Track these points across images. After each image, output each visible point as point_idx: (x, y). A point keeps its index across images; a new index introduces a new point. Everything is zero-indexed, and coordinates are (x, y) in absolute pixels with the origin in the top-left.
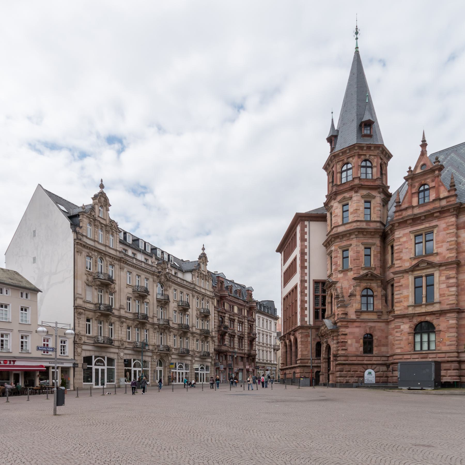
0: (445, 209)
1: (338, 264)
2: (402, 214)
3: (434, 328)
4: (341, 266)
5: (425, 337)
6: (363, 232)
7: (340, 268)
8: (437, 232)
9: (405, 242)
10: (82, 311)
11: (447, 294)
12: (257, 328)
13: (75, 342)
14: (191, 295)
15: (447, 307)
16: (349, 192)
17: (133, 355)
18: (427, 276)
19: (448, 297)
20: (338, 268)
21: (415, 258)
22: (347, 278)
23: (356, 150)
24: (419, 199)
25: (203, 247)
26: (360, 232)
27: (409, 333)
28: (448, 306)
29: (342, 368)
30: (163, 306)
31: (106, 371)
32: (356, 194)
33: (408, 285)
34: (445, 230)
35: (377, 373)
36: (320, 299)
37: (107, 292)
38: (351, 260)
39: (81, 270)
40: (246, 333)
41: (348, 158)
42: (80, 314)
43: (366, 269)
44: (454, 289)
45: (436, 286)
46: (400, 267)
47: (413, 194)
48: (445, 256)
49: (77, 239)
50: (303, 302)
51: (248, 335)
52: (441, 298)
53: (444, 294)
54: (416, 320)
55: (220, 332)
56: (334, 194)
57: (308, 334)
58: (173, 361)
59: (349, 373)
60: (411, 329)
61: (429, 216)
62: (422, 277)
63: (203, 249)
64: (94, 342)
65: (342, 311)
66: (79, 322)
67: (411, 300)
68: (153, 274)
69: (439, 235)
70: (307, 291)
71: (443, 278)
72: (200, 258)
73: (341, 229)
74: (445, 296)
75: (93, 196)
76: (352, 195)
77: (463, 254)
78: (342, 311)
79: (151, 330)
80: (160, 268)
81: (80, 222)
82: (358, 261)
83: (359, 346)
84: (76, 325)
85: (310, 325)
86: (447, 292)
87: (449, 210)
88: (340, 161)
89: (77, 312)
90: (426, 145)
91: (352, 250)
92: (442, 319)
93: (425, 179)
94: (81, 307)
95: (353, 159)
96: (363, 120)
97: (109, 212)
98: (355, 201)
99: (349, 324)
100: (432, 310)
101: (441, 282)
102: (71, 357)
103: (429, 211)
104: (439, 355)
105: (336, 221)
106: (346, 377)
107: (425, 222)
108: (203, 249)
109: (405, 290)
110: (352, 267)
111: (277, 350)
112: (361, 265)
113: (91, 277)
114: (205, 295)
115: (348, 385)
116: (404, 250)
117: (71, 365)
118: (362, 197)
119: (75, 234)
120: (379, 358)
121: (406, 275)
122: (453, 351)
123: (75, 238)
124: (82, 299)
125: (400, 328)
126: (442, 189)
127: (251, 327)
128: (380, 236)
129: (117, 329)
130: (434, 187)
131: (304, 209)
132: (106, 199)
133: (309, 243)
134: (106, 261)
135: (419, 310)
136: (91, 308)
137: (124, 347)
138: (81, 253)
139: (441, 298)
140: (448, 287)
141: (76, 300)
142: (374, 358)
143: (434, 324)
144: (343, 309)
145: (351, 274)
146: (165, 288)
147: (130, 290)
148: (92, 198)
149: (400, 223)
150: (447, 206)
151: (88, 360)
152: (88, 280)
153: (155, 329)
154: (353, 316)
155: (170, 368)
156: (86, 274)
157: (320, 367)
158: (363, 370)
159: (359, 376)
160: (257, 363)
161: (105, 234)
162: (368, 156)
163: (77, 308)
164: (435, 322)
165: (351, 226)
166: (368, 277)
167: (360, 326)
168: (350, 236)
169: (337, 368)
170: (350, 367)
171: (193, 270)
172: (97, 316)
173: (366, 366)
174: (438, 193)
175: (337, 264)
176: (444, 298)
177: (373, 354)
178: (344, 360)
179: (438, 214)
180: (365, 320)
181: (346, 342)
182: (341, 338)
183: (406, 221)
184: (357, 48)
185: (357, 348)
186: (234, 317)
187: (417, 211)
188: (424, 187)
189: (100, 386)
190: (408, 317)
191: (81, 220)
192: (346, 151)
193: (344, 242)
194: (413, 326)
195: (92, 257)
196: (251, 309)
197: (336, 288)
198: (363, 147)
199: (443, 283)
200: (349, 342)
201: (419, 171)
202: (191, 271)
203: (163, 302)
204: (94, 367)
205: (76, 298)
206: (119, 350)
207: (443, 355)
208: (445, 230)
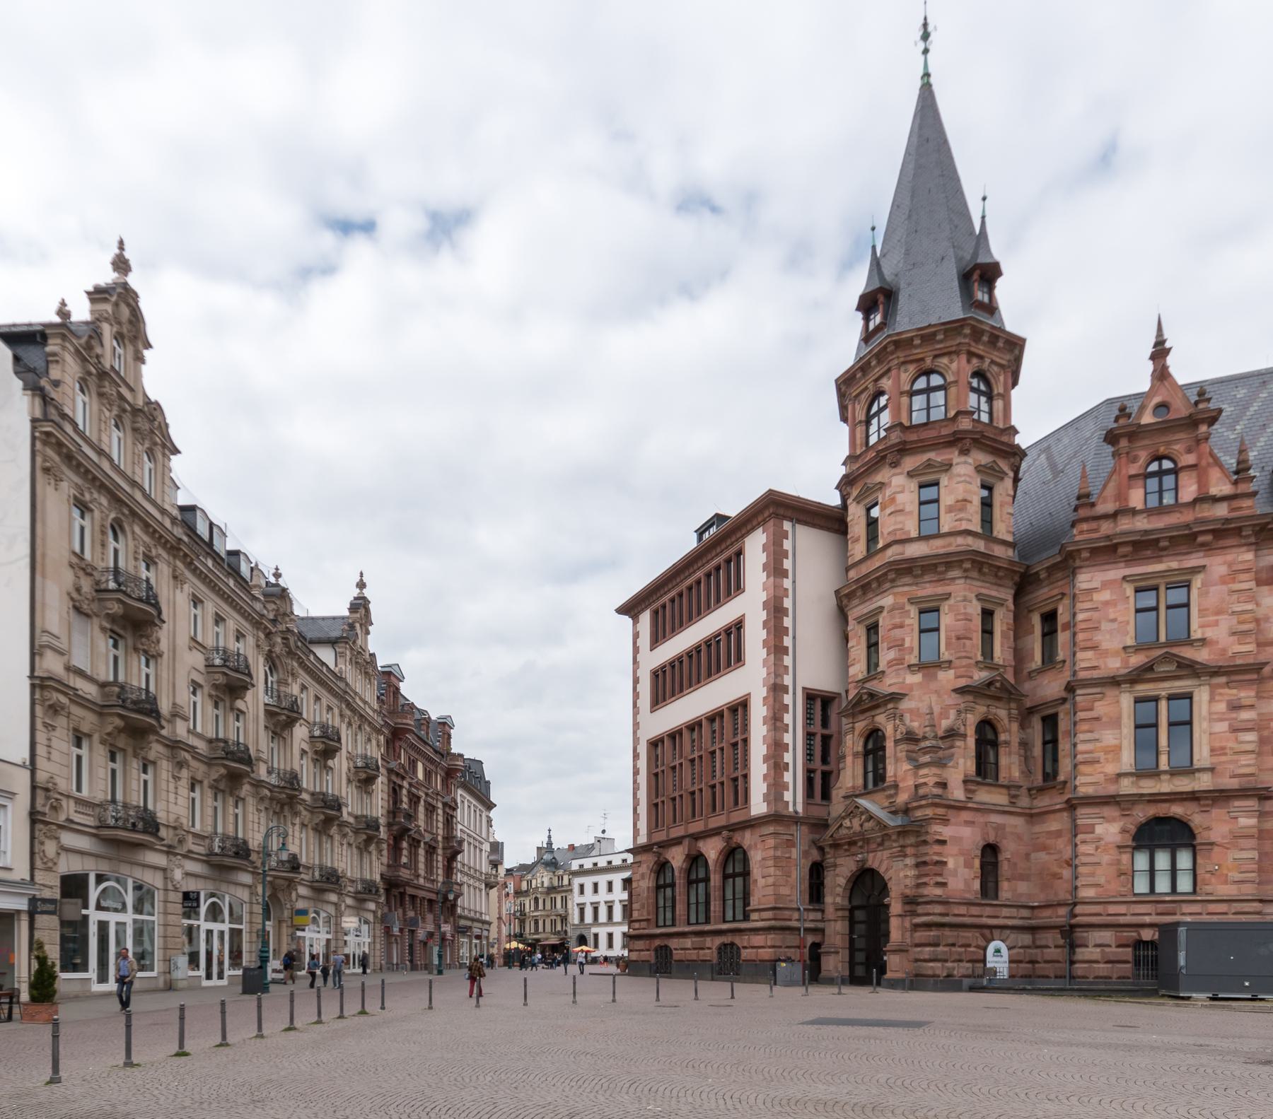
0: (1233, 526)
1: (907, 644)
3: (1193, 835)
4: (916, 652)
5: (1162, 860)
7: (912, 657)
9: (1107, 603)
10: (63, 699)
11: (1231, 749)
12: (460, 827)
13: (35, 818)
15: (1233, 784)
16: (941, 451)
17: (205, 878)
18: (1171, 698)
19: (1235, 757)
20: (907, 657)
21: (1138, 649)
22: (933, 686)
23: (965, 336)
24: (1146, 494)
25: (361, 580)
26: (979, 564)
27: (1119, 847)
28: (1236, 780)
29: (938, 936)
30: (278, 730)
31: (130, 931)
32: (963, 459)
33: (1119, 718)
34: (1223, 581)
36: (818, 741)
37: (136, 650)
38: (948, 638)
39: (57, 551)
40: (440, 838)
41: (936, 357)
42: (55, 709)
43: (1138, 649)
44: (1251, 737)
46: (1094, 668)
47: (1131, 477)
48: (1224, 650)
49: (46, 418)
51: (443, 843)
52: (1215, 760)
53: (1223, 748)
54: (1142, 814)
55: (395, 828)
56: (897, 451)
57: (789, 837)
58: (301, 905)
59: (953, 949)
60: (1127, 835)
61: (1187, 539)
62: (1156, 699)
63: (361, 585)
64: (97, 824)
65: (935, 775)
66: (49, 740)
67: (1127, 760)
69: (1207, 593)
70: (788, 718)
71: (1221, 707)
72: (354, 608)
73: (916, 550)
74: (1225, 754)
75: (91, 289)
76: (951, 459)
77: (1267, 648)
78: (935, 775)
79: (251, 801)
80: (273, 610)
81: (48, 362)
83: (972, 876)
84: (41, 750)
85: (796, 812)
86: (1230, 744)
87: (1240, 529)
88: (911, 362)
89: (43, 700)
92: (1217, 812)
93: (1169, 443)
94: (59, 682)
95: (951, 361)
98: (959, 475)
99: (951, 814)
100: (1188, 788)
101: (1215, 717)
102: (22, 872)
103: (1188, 525)
104: (1213, 908)
105: (899, 526)
107: (1167, 556)
109: (1108, 732)
110: (951, 658)
112: (976, 655)
114: (366, 719)
115: (949, 984)
116: (1105, 626)
117: (22, 904)
118: (979, 469)
119: (38, 401)
120: (1013, 912)
121: (1111, 692)
122: (1250, 898)
123: (38, 414)
125: (1093, 832)
126: (1215, 474)
127: (449, 821)
128: (1015, 584)
129: (164, 785)
132: (136, 318)
133: (794, 582)
134: (134, 539)
135: (1149, 787)
136: (88, 697)
138: (58, 480)
139: (1215, 760)
140: (1235, 730)
141: (41, 655)
142: (1005, 912)
143: (1192, 825)
144: (934, 770)
145: (947, 678)
146: (281, 676)
147: (198, 659)
148: (88, 293)
149: (1095, 551)
150: (1227, 521)
151: (74, 886)
152: (78, 590)
153: (262, 799)
154: (958, 793)
156: (71, 566)
157: (822, 931)
158: (982, 943)
159: (975, 958)
160: (461, 917)
161: (129, 441)
162: (987, 361)
163: (43, 687)
164: (1196, 817)
165: (950, 545)
166: (992, 688)
168: (946, 571)
170: (955, 933)
171: (337, 638)
172: (110, 729)
173: (989, 930)
174: (1202, 482)
175: (902, 645)
176: (1223, 758)
177: (996, 897)
178: (941, 914)
179: (1209, 538)
180: (986, 807)
181: (945, 863)
182: (932, 852)
183: (1114, 548)
184: (927, 75)
186: (418, 789)
187: (1142, 523)
188: (1160, 465)
190: (1118, 803)
191: (54, 354)
192: (934, 334)
193: (928, 585)
194: (1133, 827)
196: (449, 774)
197: (898, 711)
198: (982, 332)
199: (1221, 720)
200: (951, 864)
201: (1147, 419)
203: (284, 717)
204: (94, 916)
205: (41, 646)
206: (171, 857)
207: (1222, 908)
208: (1223, 581)
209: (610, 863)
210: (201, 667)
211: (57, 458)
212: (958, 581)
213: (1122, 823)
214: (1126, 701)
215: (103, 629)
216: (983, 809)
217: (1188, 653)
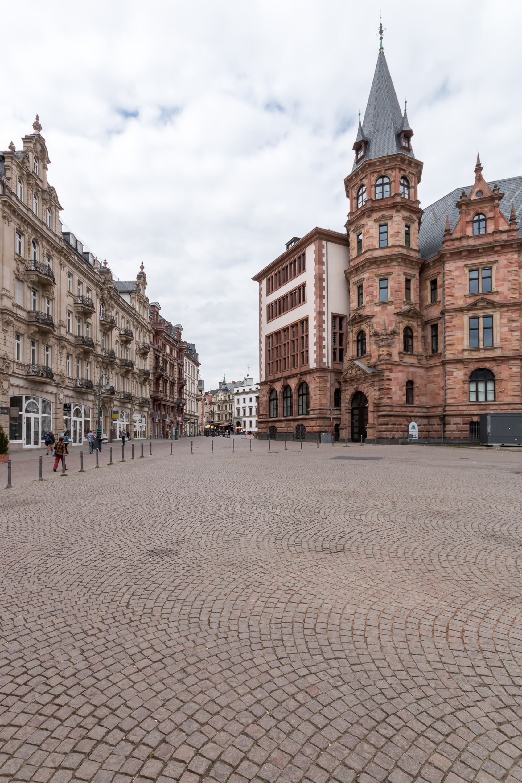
1: (374, 294)
2: (454, 243)
3: (493, 376)
4: (378, 297)
5: (481, 387)
6: (406, 259)
8: (497, 268)
9: (457, 276)
14: (131, 323)
15: (510, 354)
18: (484, 317)
19: (511, 342)
21: (471, 296)
22: (386, 312)
23: (398, 161)
24: (473, 229)
26: (404, 259)
27: (463, 381)
28: (511, 352)
30: (106, 332)
32: (397, 214)
33: (463, 326)
34: (505, 267)
35: (420, 427)
36: (338, 336)
37: (43, 296)
38: (391, 292)
40: (176, 379)
41: (386, 170)
43: (471, 296)
45: (496, 329)
48: (506, 297)
50: (320, 339)
52: (503, 343)
53: (506, 338)
54: (473, 367)
55: (157, 375)
58: (115, 409)
59: (395, 426)
61: (490, 249)
62: (478, 318)
63: (142, 267)
64: (26, 374)
66: (5, 337)
67: (466, 344)
68: (97, 284)
69: (499, 272)
70: (325, 326)
71: (505, 321)
72: (139, 277)
74: (507, 341)
79: (93, 363)
82: (400, 293)
85: (329, 367)
86: (509, 337)
87: (512, 245)
88: (376, 172)
90: (482, 168)
91: (392, 279)
92: (504, 366)
93: (482, 208)
95: (392, 172)
96: (404, 129)
97: (47, 171)
98: (396, 221)
100: (492, 356)
106: (392, 431)
108: (142, 267)
111: (199, 401)
113: (23, 265)
115: (393, 441)
116: (457, 286)
118: (404, 219)
120: (420, 410)
121: (459, 315)
124: (10, 298)
126: (501, 221)
127: (180, 371)
130: (493, 217)
131: (326, 226)
134: (43, 248)
135: (475, 355)
137: (65, 385)
139: (503, 343)
140: (511, 331)
142: (417, 410)
143: (493, 371)
145: (391, 309)
147: (71, 301)
148: (23, 139)
149: (452, 254)
151: (16, 402)
152: (18, 270)
153: (98, 362)
155: (112, 419)
156: (15, 259)
158: (407, 423)
160: (185, 414)
162: (407, 172)
165: (392, 251)
167: (403, 371)
169: (380, 420)
172: (32, 332)
173: (410, 418)
174: (496, 224)
176: (506, 343)
177: (413, 403)
178: (390, 411)
179: (499, 248)
181: (391, 389)
182: (386, 384)
183: (460, 253)
184: (382, 48)
185: (400, 397)
187: (471, 242)
188: (479, 217)
189: (32, 446)
190: (463, 362)
191: (8, 166)
192: (385, 160)
195: (24, 235)
198: (405, 160)
199: (505, 326)
200: (394, 389)
202: (129, 293)
204: (25, 415)
206: (59, 388)
207: (506, 407)
208: (505, 267)
209: (244, 390)
210: (72, 304)
211: (9, 212)
212: (396, 267)
213: (464, 371)
214: (466, 318)
215: (29, 287)
216: (407, 365)
217: (491, 298)
